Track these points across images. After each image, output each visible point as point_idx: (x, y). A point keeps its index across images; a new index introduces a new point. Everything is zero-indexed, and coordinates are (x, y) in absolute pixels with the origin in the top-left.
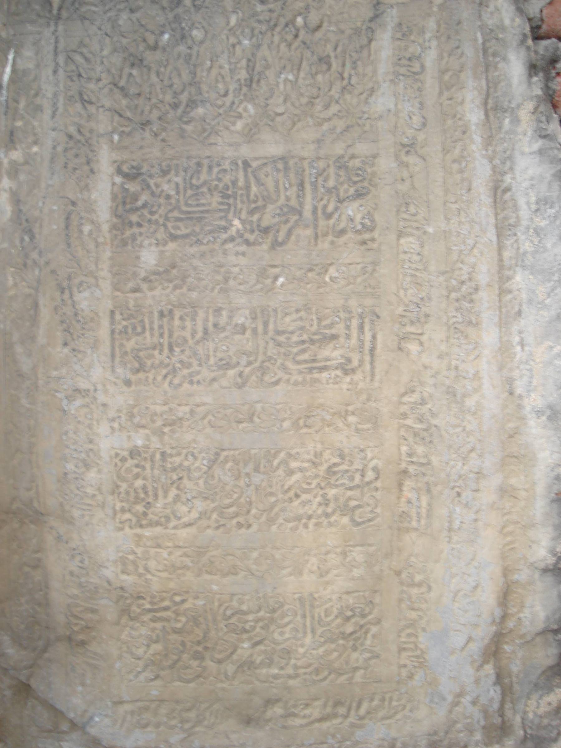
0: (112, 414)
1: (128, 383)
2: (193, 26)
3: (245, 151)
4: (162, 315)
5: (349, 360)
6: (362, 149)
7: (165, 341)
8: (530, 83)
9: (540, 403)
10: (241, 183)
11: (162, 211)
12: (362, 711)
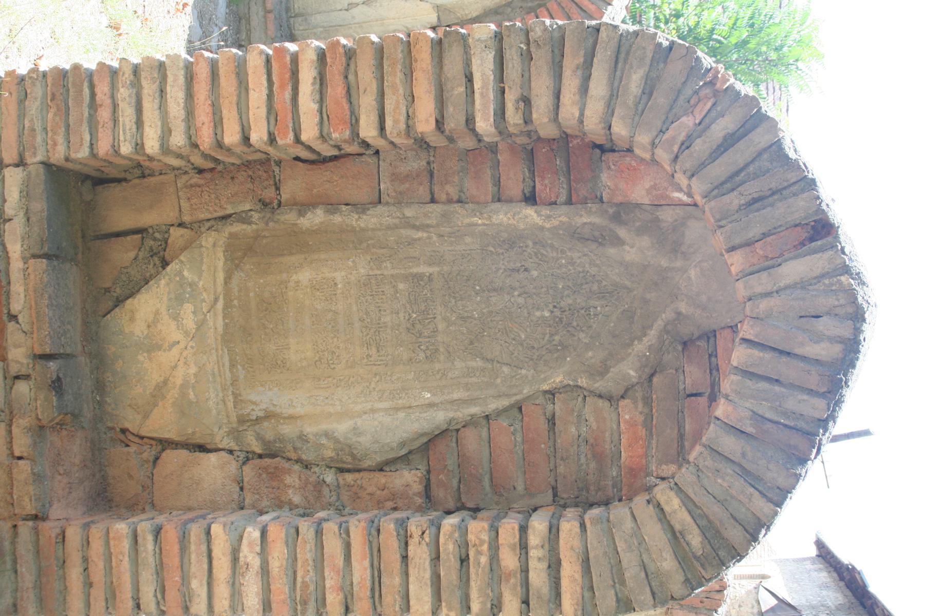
0: (349, 276)
1: (359, 281)
2: (481, 297)
3: (439, 317)
4: (383, 292)
5: (371, 357)
6: (442, 358)
7: (374, 293)
8: (469, 416)
9: (359, 424)
10: (429, 316)
11: (418, 290)
12: (249, 369)
